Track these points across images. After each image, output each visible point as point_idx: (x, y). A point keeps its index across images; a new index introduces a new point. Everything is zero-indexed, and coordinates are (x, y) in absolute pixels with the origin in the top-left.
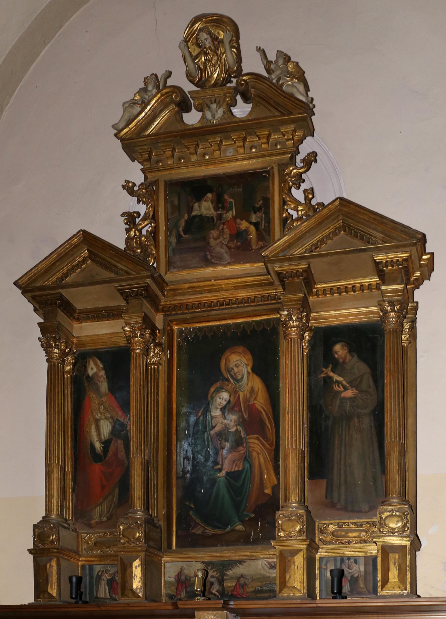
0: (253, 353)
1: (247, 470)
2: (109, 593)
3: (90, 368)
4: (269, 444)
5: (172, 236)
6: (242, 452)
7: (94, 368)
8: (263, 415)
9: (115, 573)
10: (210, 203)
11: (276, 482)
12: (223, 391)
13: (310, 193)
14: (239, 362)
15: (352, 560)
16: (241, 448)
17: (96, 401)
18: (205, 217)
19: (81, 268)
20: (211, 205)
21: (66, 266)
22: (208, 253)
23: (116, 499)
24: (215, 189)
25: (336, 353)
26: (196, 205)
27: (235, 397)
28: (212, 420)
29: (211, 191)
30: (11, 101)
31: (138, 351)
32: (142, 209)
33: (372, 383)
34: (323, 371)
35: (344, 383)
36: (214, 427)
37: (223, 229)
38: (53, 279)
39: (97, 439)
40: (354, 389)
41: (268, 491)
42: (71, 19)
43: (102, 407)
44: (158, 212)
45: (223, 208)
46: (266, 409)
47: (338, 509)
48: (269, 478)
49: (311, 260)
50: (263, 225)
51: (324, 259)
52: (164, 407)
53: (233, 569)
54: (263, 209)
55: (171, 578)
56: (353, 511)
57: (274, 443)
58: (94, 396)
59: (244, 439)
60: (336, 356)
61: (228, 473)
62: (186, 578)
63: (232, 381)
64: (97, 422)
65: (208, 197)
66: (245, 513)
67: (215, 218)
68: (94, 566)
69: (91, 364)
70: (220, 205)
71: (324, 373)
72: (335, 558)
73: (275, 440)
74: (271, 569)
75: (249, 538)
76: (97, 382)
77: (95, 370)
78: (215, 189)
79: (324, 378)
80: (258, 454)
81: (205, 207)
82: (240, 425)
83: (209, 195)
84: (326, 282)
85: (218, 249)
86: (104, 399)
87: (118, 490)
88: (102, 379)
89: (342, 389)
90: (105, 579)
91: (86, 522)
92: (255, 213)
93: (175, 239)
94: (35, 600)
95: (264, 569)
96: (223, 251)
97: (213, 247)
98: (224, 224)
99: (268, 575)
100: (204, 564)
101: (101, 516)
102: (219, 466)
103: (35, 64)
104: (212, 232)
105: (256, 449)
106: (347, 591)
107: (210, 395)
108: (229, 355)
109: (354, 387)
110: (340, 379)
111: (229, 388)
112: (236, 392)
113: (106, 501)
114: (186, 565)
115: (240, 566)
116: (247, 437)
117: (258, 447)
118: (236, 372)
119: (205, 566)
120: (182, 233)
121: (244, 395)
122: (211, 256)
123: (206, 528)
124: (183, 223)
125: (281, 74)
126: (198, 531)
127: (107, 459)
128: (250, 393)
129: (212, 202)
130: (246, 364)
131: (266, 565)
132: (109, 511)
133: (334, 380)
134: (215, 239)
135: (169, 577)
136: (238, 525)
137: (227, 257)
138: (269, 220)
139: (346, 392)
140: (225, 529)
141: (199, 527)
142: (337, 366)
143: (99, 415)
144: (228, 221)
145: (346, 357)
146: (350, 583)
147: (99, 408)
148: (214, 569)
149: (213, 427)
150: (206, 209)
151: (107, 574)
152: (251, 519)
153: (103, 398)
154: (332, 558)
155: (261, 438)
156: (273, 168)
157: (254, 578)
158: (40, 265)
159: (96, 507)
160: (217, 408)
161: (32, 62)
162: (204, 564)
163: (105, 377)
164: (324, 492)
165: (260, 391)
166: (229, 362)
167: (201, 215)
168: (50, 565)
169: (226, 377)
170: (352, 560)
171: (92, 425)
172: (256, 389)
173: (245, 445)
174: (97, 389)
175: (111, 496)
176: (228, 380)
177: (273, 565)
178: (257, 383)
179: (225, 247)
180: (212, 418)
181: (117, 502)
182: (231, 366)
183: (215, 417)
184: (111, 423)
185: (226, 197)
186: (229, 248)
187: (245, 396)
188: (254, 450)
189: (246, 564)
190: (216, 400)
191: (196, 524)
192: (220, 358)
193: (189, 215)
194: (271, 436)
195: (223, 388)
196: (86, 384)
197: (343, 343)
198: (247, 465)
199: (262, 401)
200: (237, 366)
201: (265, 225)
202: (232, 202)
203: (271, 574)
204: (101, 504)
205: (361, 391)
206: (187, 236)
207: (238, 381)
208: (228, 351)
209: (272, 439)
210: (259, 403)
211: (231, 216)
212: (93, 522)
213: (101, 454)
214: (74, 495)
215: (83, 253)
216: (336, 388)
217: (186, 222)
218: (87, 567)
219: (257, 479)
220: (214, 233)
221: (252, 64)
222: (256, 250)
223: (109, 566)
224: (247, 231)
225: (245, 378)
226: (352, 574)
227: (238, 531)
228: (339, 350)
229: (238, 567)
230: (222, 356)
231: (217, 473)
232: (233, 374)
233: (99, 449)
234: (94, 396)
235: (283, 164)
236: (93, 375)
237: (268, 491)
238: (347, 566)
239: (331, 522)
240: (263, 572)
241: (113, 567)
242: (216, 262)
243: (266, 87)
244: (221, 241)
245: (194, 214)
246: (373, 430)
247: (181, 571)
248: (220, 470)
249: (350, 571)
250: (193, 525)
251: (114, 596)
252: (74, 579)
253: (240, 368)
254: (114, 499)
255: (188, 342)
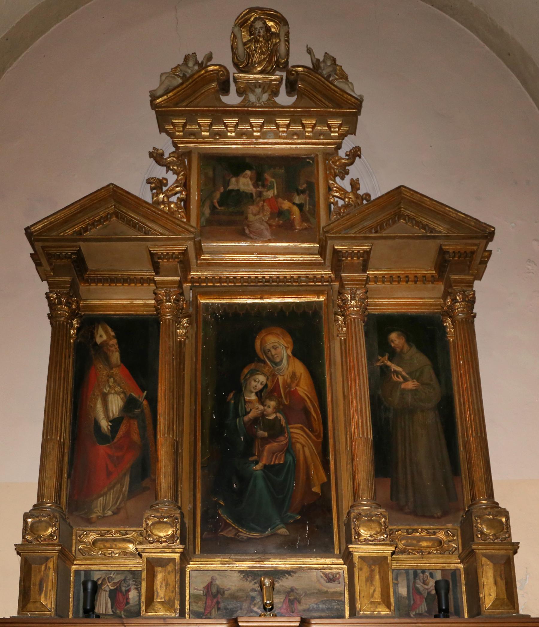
0: (292, 334)
1: (290, 465)
2: (112, 608)
3: (98, 335)
4: (315, 436)
5: (205, 207)
6: (283, 443)
7: (103, 335)
8: (307, 403)
9: (121, 581)
10: (248, 179)
11: (325, 480)
12: (259, 374)
13: (355, 184)
14: (277, 345)
15: (427, 574)
16: (282, 438)
17: (105, 373)
18: (243, 192)
19: (103, 224)
20: (250, 183)
21: (82, 221)
22: (246, 227)
23: (126, 488)
24: (255, 168)
25: (393, 342)
26: (233, 180)
27: (273, 381)
28: (245, 405)
29: (250, 168)
30: (14, 65)
31: (169, 316)
32: (172, 178)
33: (434, 376)
34: (379, 360)
35: (404, 373)
36: (249, 413)
37: (263, 206)
38: (70, 232)
39: (104, 417)
40: (415, 380)
41: (316, 489)
42: (86, 5)
43: (112, 380)
44: (190, 181)
45: (263, 186)
46: (310, 396)
47: (407, 513)
48: (318, 475)
49: (376, 242)
50: (307, 207)
51: (390, 242)
52: (191, 385)
53: (280, 581)
54: (307, 192)
55: (197, 590)
56: (424, 516)
57: (322, 435)
58: (101, 366)
59: (286, 429)
60: (393, 345)
61: (265, 466)
62: (218, 591)
63: (269, 363)
64: (105, 398)
65: (246, 174)
66: (289, 514)
67: (254, 195)
68: (92, 572)
69: (101, 331)
70: (260, 183)
71: (381, 361)
72: (407, 571)
73: (322, 432)
74: (329, 582)
75: (295, 544)
76: (106, 351)
77: (105, 337)
78: (255, 168)
79: (381, 367)
80: (303, 446)
81: (244, 183)
82: (279, 412)
83: (248, 172)
84: (378, 270)
85: (258, 225)
86: (115, 371)
87: (129, 479)
88: (113, 349)
89: (401, 380)
90: (107, 589)
91: (83, 516)
92: (299, 194)
93: (209, 209)
94: (18, 613)
95: (320, 583)
96: (263, 227)
97: (252, 222)
98: (264, 201)
99: (325, 589)
100: (241, 574)
101: (104, 509)
102: (255, 458)
103: (44, 36)
104: (251, 207)
105: (301, 440)
106: (424, 611)
107: (242, 377)
108: (265, 336)
109: (415, 379)
110: (399, 369)
111: (266, 370)
112: (274, 376)
113: (112, 491)
114: (218, 575)
115: (290, 577)
116: (289, 426)
117: (303, 438)
118: (273, 354)
119: (244, 576)
120: (217, 205)
121: (284, 379)
122: (250, 231)
123: (240, 530)
124: (217, 195)
125: (332, 71)
126: (229, 534)
127: (115, 440)
128: (291, 378)
129: (251, 179)
130: (286, 347)
131: (322, 577)
132: (116, 503)
133: (393, 370)
134: (255, 215)
135: (195, 589)
136: (280, 528)
137: (267, 234)
138: (314, 204)
139: (407, 383)
140: (265, 532)
141: (231, 528)
142: (393, 354)
143: (108, 389)
144: (269, 199)
145: (403, 347)
146: (426, 602)
147: (108, 380)
148: (256, 581)
149: (247, 413)
150: (244, 184)
151: (109, 582)
152: (296, 521)
153: (114, 369)
154: (404, 571)
155: (305, 429)
156: (317, 155)
157: (308, 592)
158: (59, 214)
159: (100, 497)
160: (252, 392)
161: (43, 33)
162: (241, 574)
163: (117, 346)
164: (388, 492)
165: (302, 376)
166: (266, 343)
167: (238, 190)
168: (46, 566)
169: (262, 358)
170: (427, 574)
171: (97, 400)
172: (298, 374)
173: (286, 435)
174: (107, 359)
175: (119, 485)
176: (264, 362)
177: (332, 577)
178: (299, 368)
179: (266, 224)
180: (245, 402)
181: (126, 493)
182: (268, 347)
183: (250, 402)
184: (122, 399)
185: (267, 176)
186: (270, 226)
187: (285, 382)
188: (298, 442)
189: (297, 575)
190: (250, 383)
191: (227, 525)
192: (254, 339)
193: (225, 188)
194: (317, 425)
195: (258, 371)
196: (93, 352)
197: (400, 333)
198: (290, 458)
199: (306, 388)
200: (275, 348)
201: (309, 208)
202: (273, 182)
203: (329, 588)
204: (106, 494)
205: (423, 384)
206: (223, 208)
207: (276, 364)
208: (263, 331)
209: (318, 430)
210: (302, 390)
211: (272, 195)
212: (94, 516)
213: (109, 434)
214: (69, 481)
215: (108, 208)
216: (395, 378)
217: (222, 195)
218: (83, 573)
219: (302, 475)
220: (252, 209)
221: (299, 59)
222: (300, 230)
223: (113, 572)
224: (289, 212)
225: (285, 361)
226: (430, 590)
227: (281, 535)
228: (396, 339)
229: (287, 578)
230: (256, 337)
231: (253, 465)
232: (271, 357)
233: (106, 429)
234: (101, 366)
235: (328, 153)
236: (101, 343)
237: (316, 489)
238: (422, 581)
239: (400, 528)
240: (318, 586)
241: (118, 574)
242: (255, 237)
243: (315, 80)
244: (261, 218)
245: (230, 188)
246: (440, 426)
247: (211, 582)
248: (257, 463)
249: (426, 587)
250: (223, 526)
251: (118, 612)
252: (90, 585)
253: (278, 350)
254: (124, 489)
255: (216, 318)
